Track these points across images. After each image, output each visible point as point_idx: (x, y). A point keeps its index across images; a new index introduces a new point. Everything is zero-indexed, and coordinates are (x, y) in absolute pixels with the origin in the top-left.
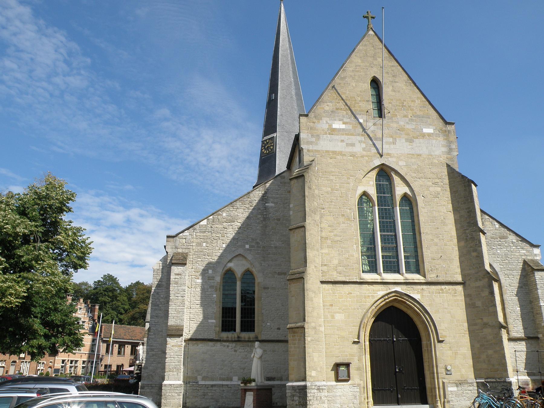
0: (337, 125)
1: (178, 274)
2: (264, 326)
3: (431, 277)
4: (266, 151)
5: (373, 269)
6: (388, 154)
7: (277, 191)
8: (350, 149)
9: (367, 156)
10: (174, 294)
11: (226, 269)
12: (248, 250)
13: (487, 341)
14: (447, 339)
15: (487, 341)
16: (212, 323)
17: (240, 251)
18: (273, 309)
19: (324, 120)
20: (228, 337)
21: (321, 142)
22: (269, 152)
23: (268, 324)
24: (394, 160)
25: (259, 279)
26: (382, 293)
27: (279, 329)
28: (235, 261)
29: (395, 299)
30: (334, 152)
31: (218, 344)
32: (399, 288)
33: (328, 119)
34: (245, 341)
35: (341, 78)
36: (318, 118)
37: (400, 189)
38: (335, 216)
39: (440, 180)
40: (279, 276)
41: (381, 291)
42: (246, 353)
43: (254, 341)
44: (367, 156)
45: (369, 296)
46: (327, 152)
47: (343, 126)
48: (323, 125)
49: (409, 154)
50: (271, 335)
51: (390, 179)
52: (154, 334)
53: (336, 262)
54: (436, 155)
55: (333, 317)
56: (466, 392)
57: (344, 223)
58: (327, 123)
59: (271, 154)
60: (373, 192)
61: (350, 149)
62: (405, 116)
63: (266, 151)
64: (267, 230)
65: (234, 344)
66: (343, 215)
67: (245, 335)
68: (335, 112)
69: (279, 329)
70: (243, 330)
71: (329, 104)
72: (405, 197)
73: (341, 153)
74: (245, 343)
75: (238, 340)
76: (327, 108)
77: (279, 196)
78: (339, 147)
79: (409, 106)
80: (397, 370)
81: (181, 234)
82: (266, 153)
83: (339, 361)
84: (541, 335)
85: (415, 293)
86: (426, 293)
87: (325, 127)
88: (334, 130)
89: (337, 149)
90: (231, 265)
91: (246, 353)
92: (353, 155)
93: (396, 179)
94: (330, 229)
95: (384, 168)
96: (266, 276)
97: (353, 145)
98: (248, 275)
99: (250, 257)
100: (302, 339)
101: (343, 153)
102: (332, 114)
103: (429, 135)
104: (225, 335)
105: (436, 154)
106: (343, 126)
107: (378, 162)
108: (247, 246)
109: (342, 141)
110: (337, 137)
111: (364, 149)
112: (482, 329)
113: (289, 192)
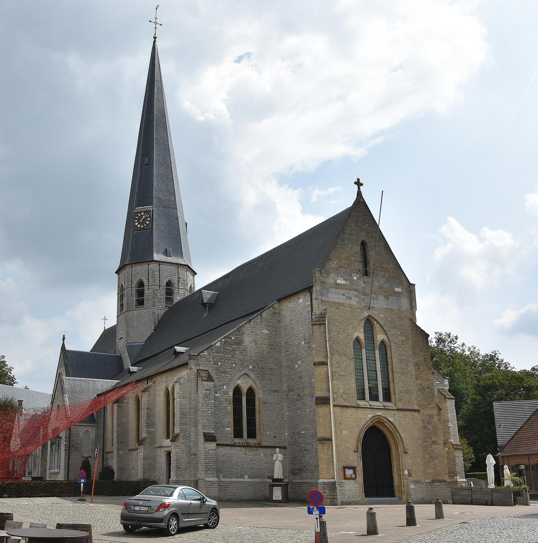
0: (340, 281)
1: (208, 390)
2: (264, 434)
3: (400, 405)
4: (141, 226)
5: (362, 397)
6: (373, 308)
7: (270, 320)
8: (348, 302)
9: (359, 308)
10: (206, 406)
11: (235, 385)
12: (251, 370)
13: (434, 454)
14: (409, 452)
15: (434, 454)
16: (228, 430)
17: (246, 371)
18: (271, 421)
19: (332, 275)
20: (240, 443)
21: (330, 295)
22: (144, 227)
23: (268, 433)
24: (377, 312)
25: (259, 395)
26: (370, 416)
27: (275, 437)
28: (241, 379)
29: (378, 421)
30: (338, 303)
31: (233, 448)
32: (379, 413)
33: (333, 275)
34: (252, 447)
35: (342, 240)
36: (328, 273)
37: (380, 337)
38: (340, 355)
39: (405, 331)
40: (273, 394)
41: (370, 415)
42: (253, 456)
43: (275, 447)
44: (359, 308)
45: (362, 418)
46: (334, 302)
47: (344, 282)
48: (330, 280)
49: (385, 308)
50: (269, 442)
51: (372, 326)
52: (183, 439)
53: (341, 391)
54: (403, 311)
55: (341, 433)
56: (420, 488)
57: (346, 361)
58: (333, 278)
59: (146, 229)
60: (362, 336)
61: (348, 302)
62: (384, 277)
63: (141, 226)
64: (264, 354)
65: (244, 449)
66: (345, 355)
67: (251, 441)
68: (338, 269)
69: (275, 437)
70: (248, 437)
71: (334, 262)
72: (383, 342)
73: (342, 304)
74: (252, 448)
75: (248, 446)
76: (333, 266)
77: (272, 325)
78: (342, 299)
79: (386, 268)
80: (377, 473)
81: (202, 354)
82: (140, 227)
83: (345, 466)
84: (447, 448)
85: (392, 417)
86: (396, 417)
87: (332, 281)
88: (338, 284)
89: (341, 301)
90: (239, 382)
91: (253, 456)
92: (351, 306)
93: (377, 327)
94: (337, 365)
95: (370, 318)
96: (265, 393)
97: (350, 298)
98: (251, 392)
99: (253, 376)
100: (330, 448)
101: (344, 305)
102: (337, 270)
103: (399, 293)
104: (237, 441)
105: (403, 309)
106: (344, 282)
107: (366, 314)
108: (251, 367)
109: (344, 295)
110: (340, 291)
111: (358, 302)
112: (431, 445)
113: (279, 321)
